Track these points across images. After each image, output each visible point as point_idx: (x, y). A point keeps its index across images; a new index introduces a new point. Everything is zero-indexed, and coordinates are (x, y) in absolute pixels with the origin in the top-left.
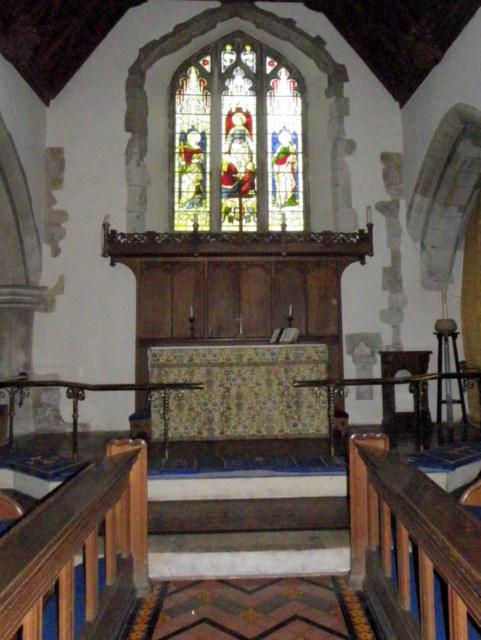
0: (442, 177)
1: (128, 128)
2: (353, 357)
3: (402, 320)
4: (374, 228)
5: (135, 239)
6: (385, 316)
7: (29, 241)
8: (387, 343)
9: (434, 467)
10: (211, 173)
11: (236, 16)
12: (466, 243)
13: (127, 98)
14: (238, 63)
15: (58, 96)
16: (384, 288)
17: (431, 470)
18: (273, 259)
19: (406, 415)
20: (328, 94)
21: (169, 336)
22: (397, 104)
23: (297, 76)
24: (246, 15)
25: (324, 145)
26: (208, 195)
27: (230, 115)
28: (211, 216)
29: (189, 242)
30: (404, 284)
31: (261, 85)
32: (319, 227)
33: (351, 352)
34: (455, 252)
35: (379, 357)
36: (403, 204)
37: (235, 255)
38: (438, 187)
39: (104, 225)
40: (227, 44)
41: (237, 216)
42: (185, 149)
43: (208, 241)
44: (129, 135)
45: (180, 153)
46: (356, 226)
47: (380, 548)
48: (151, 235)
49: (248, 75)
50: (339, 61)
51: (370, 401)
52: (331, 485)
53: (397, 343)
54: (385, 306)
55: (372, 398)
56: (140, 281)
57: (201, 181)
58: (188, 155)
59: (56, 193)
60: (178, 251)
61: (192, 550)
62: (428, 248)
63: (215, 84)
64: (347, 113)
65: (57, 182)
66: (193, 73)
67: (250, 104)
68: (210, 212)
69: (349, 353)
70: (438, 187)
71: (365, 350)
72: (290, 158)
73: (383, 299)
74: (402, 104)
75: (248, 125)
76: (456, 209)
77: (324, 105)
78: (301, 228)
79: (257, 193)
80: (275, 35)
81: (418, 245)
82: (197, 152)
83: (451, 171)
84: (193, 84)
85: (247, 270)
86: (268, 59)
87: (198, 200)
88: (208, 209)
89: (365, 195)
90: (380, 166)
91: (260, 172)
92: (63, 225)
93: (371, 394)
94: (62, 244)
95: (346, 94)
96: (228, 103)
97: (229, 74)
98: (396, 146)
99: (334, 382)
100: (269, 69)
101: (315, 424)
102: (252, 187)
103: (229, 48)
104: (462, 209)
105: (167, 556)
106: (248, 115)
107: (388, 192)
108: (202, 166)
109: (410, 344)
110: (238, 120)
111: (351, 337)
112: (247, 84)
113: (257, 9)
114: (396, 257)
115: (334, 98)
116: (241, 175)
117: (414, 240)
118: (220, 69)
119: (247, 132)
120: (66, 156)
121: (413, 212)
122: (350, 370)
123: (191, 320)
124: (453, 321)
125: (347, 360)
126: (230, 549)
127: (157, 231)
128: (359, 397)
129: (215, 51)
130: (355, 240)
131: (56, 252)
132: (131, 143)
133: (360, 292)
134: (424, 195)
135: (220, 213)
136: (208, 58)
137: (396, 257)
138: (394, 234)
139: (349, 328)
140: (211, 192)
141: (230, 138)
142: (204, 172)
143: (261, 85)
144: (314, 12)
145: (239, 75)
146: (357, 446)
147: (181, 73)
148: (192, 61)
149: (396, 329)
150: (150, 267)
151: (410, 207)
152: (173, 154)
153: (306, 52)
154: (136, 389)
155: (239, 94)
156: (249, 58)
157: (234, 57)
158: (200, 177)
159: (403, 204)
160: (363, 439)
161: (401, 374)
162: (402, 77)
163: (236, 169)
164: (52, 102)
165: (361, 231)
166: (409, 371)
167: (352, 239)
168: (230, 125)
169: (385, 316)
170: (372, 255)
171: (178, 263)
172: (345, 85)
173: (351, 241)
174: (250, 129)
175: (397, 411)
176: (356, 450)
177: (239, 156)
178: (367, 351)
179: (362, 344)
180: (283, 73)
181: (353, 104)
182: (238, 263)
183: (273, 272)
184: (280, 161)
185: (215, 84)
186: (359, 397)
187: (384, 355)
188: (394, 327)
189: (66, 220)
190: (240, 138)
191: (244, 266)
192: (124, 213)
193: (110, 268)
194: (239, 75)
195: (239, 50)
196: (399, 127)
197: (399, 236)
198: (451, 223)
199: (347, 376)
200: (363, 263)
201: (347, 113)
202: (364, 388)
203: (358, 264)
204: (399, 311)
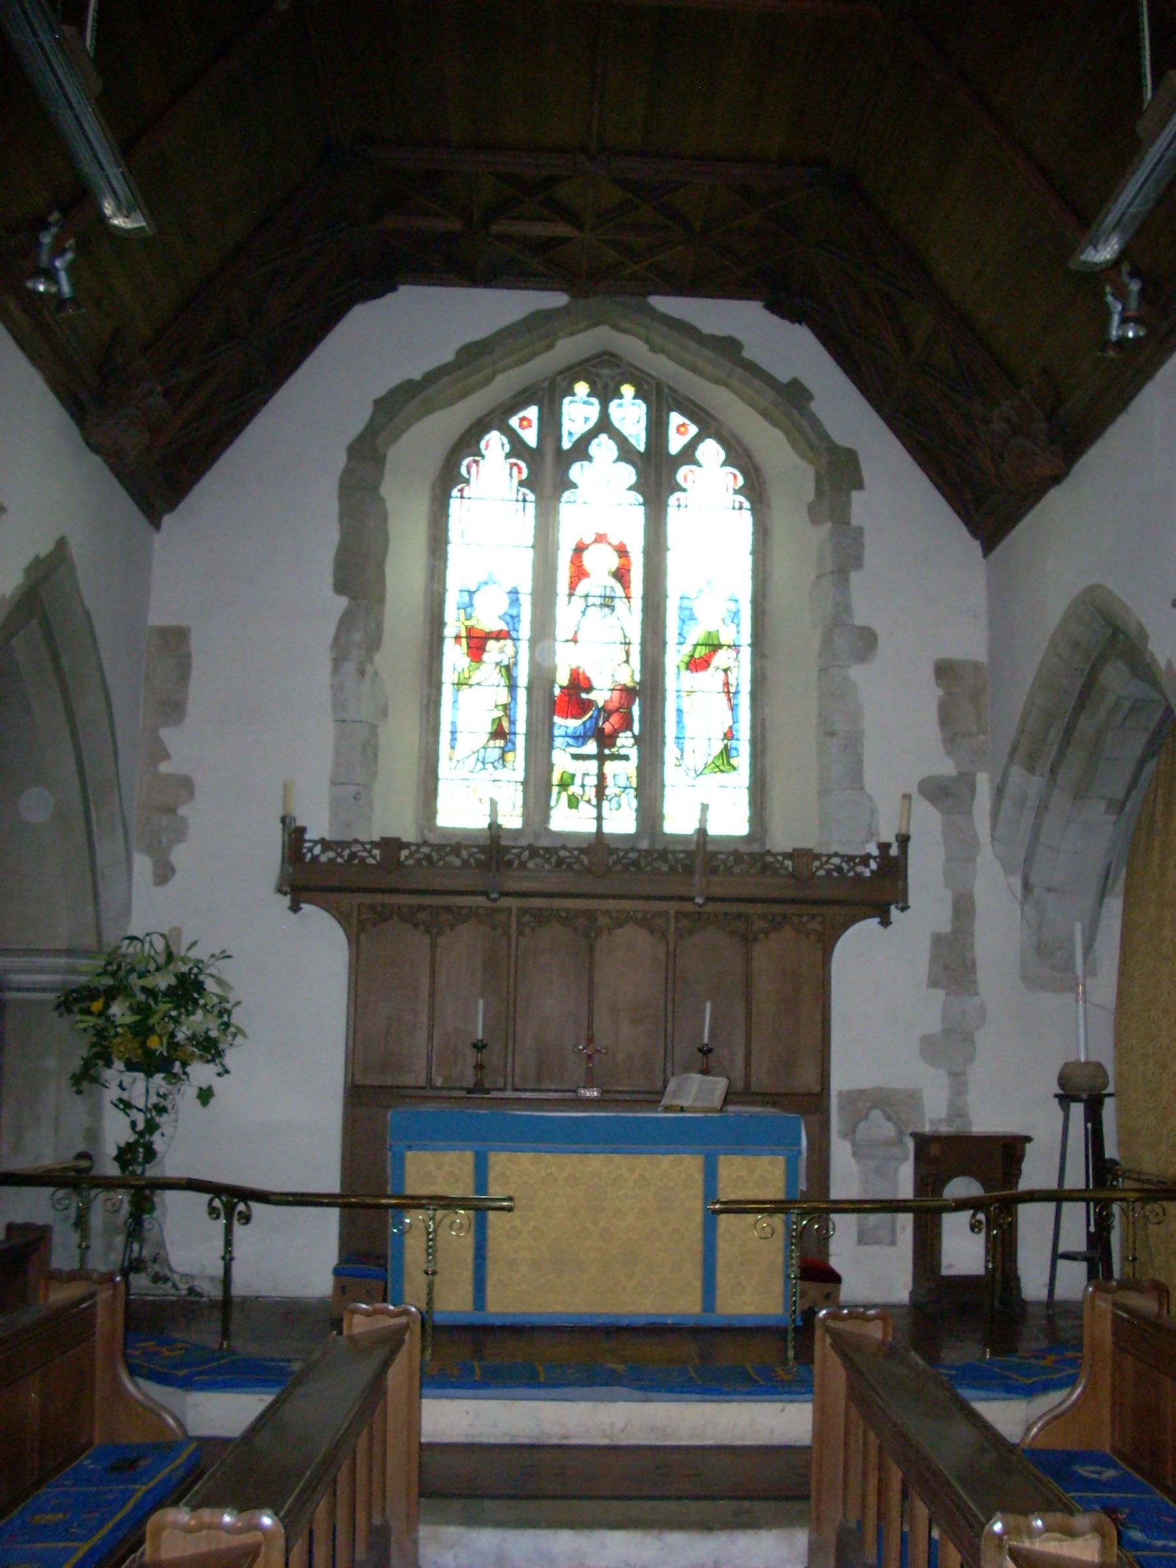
14: (604, 425)
23: (738, 455)
27: (580, 549)
31: (656, 474)
36: (984, 783)
49: (626, 452)
58: (477, 643)
63: (548, 471)
66: (494, 443)
69: (844, 1135)
72: (721, 658)
75: (622, 575)
82: (499, 636)
86: (675, 419)
91: (649, 690)
94: (180, 855)
97: (581, 450)
106: (622, 552)
108: (509, 671)
110: (600, 562)
112: (628, 474)
114: (963, 908)
116: (600, 696)
129: (549, 397)
131: (164, 873)
136: (532, 412)
137: (963, 908)
142: (512, 687)
143: (656, 474)
145: (603, 448)
147: (468, 443)
148: (496, 418)
155: (603, 493)
159: (984, 783)
168: (579, 573)
169: (931, 1049)
180: (711, 451)
184: (697, 664)
185: (548, 471)
190: (602, 605)
194: (603, 448)
195: (605, 393)
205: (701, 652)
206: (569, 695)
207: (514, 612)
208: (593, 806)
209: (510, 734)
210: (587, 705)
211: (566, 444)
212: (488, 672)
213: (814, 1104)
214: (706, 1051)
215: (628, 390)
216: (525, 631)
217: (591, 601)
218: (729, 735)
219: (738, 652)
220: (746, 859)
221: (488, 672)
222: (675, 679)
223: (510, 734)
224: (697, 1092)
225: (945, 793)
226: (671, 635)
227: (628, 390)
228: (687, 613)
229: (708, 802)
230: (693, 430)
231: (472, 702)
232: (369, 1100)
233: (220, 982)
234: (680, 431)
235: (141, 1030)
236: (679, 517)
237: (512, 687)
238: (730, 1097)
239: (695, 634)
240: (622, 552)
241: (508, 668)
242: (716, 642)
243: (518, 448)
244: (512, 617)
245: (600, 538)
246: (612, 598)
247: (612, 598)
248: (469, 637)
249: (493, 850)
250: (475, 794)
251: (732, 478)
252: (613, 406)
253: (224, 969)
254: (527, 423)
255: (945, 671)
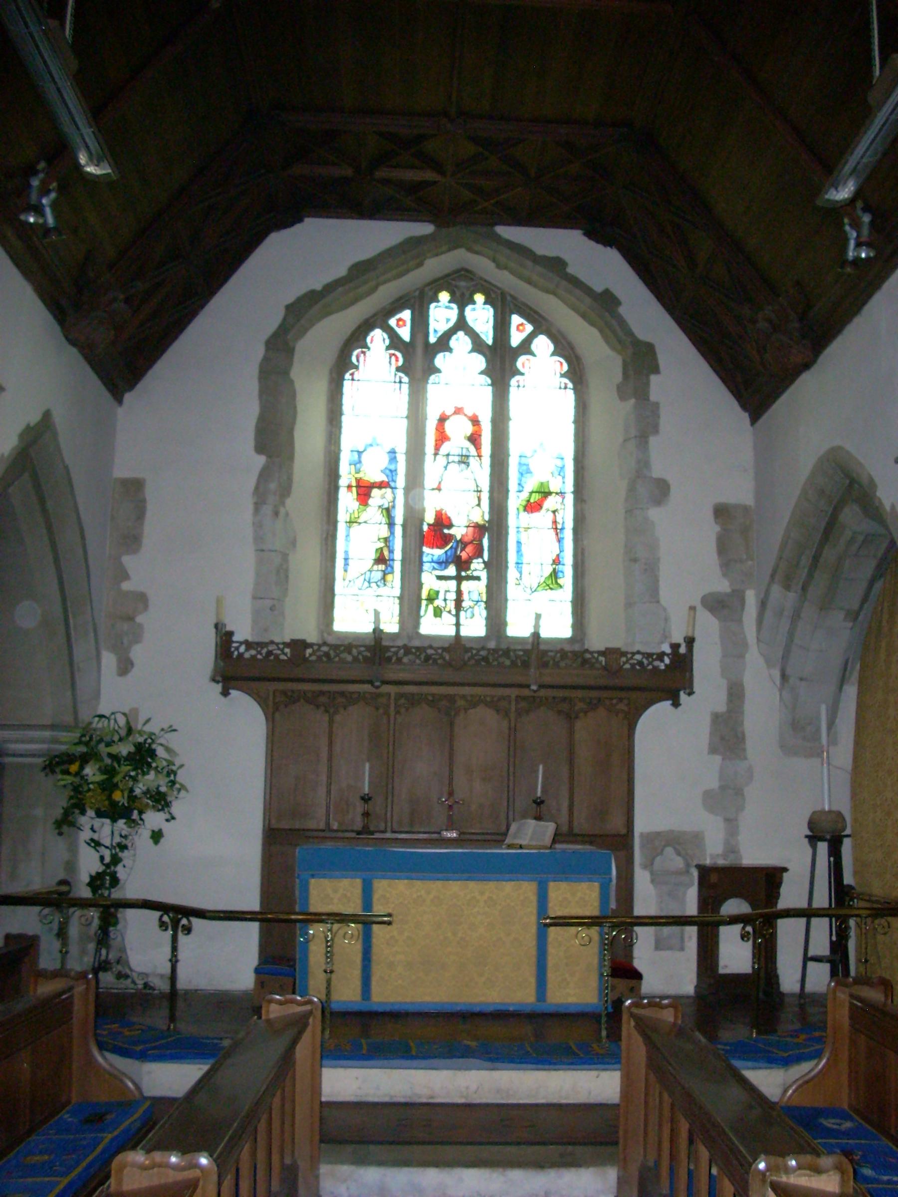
0: (816, 559)
1: (260, 448)
2: (652, 873)
3: (741, 808)
4: (696, 646)
5: (270, 653)
6: (711, 801)
7: (81, 650)
8: (713, 852)
9: (755, 1060)
10: (404, 526)
11: (461, 247)
12: (862, 670)
13: (262, 393)
14: (461, 325)
15: (139, 386)
16: (713, 750)
17: (750, 1064)
18: (513, 692)
19: (736, 979)
20: (622, 394)
21: (322, 826)
22: (745, 416)
23: (564, 347)
24: (477, 248)
25: (613, 495)
26: (397, 566)
27: (443, 419)
28: (401, 604)
29: (366, 659)
30: (749, 744)
31: (501, 362)
32: (597, 642)
33: (648, 865)
34: (840, 688)
35: (695, 873)
36: (751, 598)
37: (660, 1143)
38: (810, 576)
39: (216, 626)
40: (441, 290)
41: (451, 605)
42: (358, 481)
43: (399, 660)
44: (261, 460)
45: (349, 487)
46: (665, 636)
47: (657, 1163)
48: (299, 645)
49: (478, 345)
50: (642, 335)
51: (678, 954)
52: (598, 1085)
53: (731, 849)
54: (713, 783)
55: (682, 949)
56: (270, 719)
57: (386, 540)
58: (364, 491)
59: (128, 561)
60: (343, 675)
61: (381, 1163)
62: (791, 680)
63: (418, 359)
64: (655, 429)
65: (132, 541)
66: (377, 338)
67: (479, 398)
68: (401, 598)
69: (645, 867)
70: (810, 576)
71: (672, 860)
72: (551, 503)
73: (709, 771)
74: (755, 418)
75: (475, 439)
76: (841, 615)
77: (615, 414)
78: (566, 632)
79: (487, 565)
80: (529, 282)
81: (777, 674)
82: (381, 485)
83: (829, 555)
84: (376, 360)
85: (466, 710)
86: (516, 320)
87: (379, 575)
88: (397, 592)
89: (689, 562)
90: (712, 529)
91: (495, 527)
92: (139, 619)
93: (682, 939)
94: (137, 653)
95: (653, 397)
96: (440, 395)
97: (443, 344)
98: (740, 491)
99: (617, 923)
100: (516, 339)
101: (576, 983)
102: (479, 553)
103: (444, 296)
104: (853, 616)
105: (345, 1169)
106: (475, 421)
107: (725, 575)
108: (388, 512)
109: (754, 855)
110: (458, 429)
111: (651, 838)
112: (479, 362)
113: (498, 239)
114: (736, 693)
115: (633, 401)
116: (458, 531)
117: (769, 663)
118: (427, 335)
119: (473, 451)
120: (150, 493)
121: (768, 613)
122: (647, 899)
123: (366, 799)
124: (839, 814)
125: (642, 879)
126: (436, 1164)
127: (309, 641)
128: (659, 945)
129: (419, 303)
130: (662, 667)
131: (125, 666)
132: (264, 475)
133: (668, 748)
134: (787, 587)
135: (419, 600)
136: (406, 315)
137: (736, 693)
138: (733, 650)
139: (644, 823)
140: (403, 561)
141: (441, 460)
142: (391, 525)
143: (501, 362)
144: (600, 247)
145: (461, 342)
146: (632, 1015)
147: (357, 338)
148: (379, 319)
149: (732, 824)
150: (292, 699)
151: (763, 605)
152: (336, 488)
153: (584, 316)
154: (261, 921)
155: (460, 377)
156: (481, 316)
157: (453, 314)
158: (384, 532)
159: (751, 598)
160: (644, 1007)
161: (734, 906)
162: (754, 382)
163: (449, 519)
164: (128, 397)
165: (675, 647)
166: (746, 899)
167: (657, 663)
168: (442, 438)
169: (711, 801)
170: (691, 693)
171: (342, 694)
172: (653, 378)
173: (656, 668)
174: (478, 447)
175: (722, 971)
176: (633, 1023)
177: (457, 495)
178: (679, 863)
179: (669, 850)
180: (543, 344)
181: (665, 421)
182: (451, 699)
183: (513, 716)
184: (532, 507)
185: (418, 359)
186: (659, 945)
187: (705, 872)
188: (727, 820)
189: (146, 607)
190: (460, 462)
191: (461, 703)
192: (148, 498)
193: (222, 698)
194: (461, 342)
195: (462, 300)
196: (747, 455)
197: (741, 656)
198: (829, 640)
199: (639, 910)
200: (676, 704)
201: (656, 430)
202: (666, 930)
203: (666, 705)
204: (739, 792)
205: (535, 498)
206: (435, 531)
207: (392, 467)
208: (453, 616)
209: (389, 560)
210: (449, 538)
211: (432, 339)
212: (373, 513)
213: (621, 843)
214: (539, 803)
215: (479, 298)
216: (401, 481)
217: (451, 458)
218: (557, 561)
219: (564, 498)
220: (569, 655)
221: (373, 513)
222: (516, 518)
223: (389, 560)
224: (532, 834)
225: (722, 606)
226: (513, 485)
227: (479, 298)
228: (525, 468)
229: (541, 612)
230: (529, 328)
231: (361, 536)
232: (282, 840)
233: (168, 749)
234: (519, 329)
235: (108, 787)
236: (519, 395)
237: (391, 525)
238: (557, 838)
239: (531, 484)
240: (475, 421)
241: (388, 510)
242: (547, 490)
243: (395, 342)
244: (391, 471)
245: (458, 411)
246: (468, 456)
247: (468, 456)
248: (358, 486)
249: (376, 649)
250: (362, 606)
251: (559, 365)
252: (468, 310)
253: (171, 739)
254: (403, 323)
255: (721, 512)
